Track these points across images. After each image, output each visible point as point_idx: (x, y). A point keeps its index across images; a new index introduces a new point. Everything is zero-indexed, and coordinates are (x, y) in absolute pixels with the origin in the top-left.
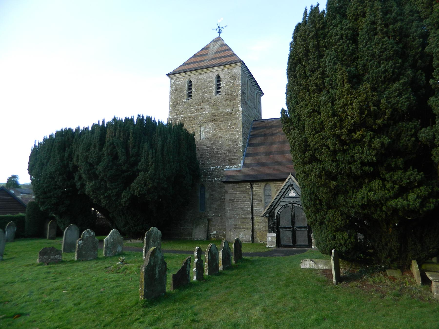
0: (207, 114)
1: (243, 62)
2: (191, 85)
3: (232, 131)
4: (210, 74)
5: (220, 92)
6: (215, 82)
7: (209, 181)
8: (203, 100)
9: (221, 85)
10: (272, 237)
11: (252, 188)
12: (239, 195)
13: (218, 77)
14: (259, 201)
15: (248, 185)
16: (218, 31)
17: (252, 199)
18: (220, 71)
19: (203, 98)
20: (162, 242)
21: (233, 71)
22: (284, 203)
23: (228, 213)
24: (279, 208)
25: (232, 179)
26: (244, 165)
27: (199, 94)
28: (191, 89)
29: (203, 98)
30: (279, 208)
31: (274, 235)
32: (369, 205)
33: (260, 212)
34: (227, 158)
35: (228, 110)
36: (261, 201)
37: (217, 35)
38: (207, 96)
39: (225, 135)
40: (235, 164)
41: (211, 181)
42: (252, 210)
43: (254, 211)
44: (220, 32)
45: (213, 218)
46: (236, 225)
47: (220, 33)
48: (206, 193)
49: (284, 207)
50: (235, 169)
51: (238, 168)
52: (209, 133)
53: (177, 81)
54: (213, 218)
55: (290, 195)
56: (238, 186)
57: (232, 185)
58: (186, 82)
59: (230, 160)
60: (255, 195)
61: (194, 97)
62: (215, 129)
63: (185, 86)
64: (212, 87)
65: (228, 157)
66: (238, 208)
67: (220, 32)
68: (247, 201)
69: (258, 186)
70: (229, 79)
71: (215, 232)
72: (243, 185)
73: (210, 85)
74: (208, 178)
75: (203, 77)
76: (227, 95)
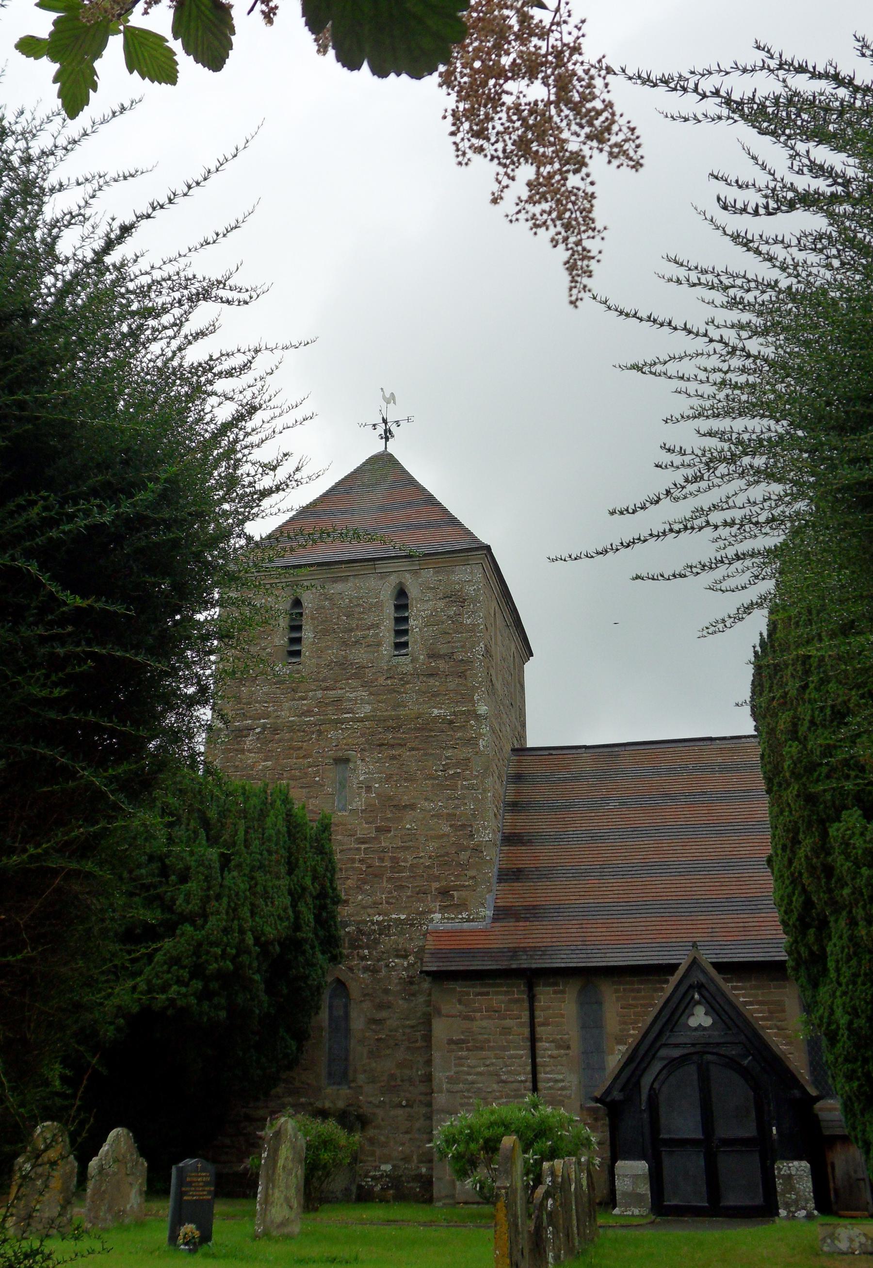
0: (361, 720)
1: (488, 548)
3: (454, 788)
4: (372, 582)
5: (405, 645)
6: (389, 611)
7: (366, 969)
8: (349, 672)
9: (411, 622)
10: (636, 1177)
11: (532, 999)
12: (484, 1023)
13: (401, 592)
14: (559, 1047)
15: (519, 992)
16: (381, 430)
17: (533, 1039)
18: (408, 575)
19: (343, 664)
21: (455, 578)
22: (676, 1053)
23: (440, 1091)
24: (657, 1066)
26: (502, 913)
27: (328, 647)
29: (343, 664)
30: (657, 1066)
31: (641, 1167)
33: (563, 1089)
34: (435, 885)
35: (436, 712)
36: (568, 1048)
37: (378, 447)
38: (359, 655)
39: (426, 799)
40: (462, 906)
41: (374, 971)
44: (387, 435)
45: (380, 1112)
47: (387, 439)
48: (353, 1014)
49: (674, 1064)
50: (466, 925)
52: (369, 789)
54: (380, 1112)
55: (693, 1022)
56: (478, 990)
57: (458, 987)
58: (283, 604)
59: (444, 893)
60: (543, 1024)
62: (389, 777)
64: (377, 626)
65: (437, 878)
67: (387, 435)
68: (516, 1048)
69: (555, 992)
70: (441, 604)
71: (387, 1168)
72: (501, 985)
73: (371, 619)
74: (363, 958)
75: (345, 590)
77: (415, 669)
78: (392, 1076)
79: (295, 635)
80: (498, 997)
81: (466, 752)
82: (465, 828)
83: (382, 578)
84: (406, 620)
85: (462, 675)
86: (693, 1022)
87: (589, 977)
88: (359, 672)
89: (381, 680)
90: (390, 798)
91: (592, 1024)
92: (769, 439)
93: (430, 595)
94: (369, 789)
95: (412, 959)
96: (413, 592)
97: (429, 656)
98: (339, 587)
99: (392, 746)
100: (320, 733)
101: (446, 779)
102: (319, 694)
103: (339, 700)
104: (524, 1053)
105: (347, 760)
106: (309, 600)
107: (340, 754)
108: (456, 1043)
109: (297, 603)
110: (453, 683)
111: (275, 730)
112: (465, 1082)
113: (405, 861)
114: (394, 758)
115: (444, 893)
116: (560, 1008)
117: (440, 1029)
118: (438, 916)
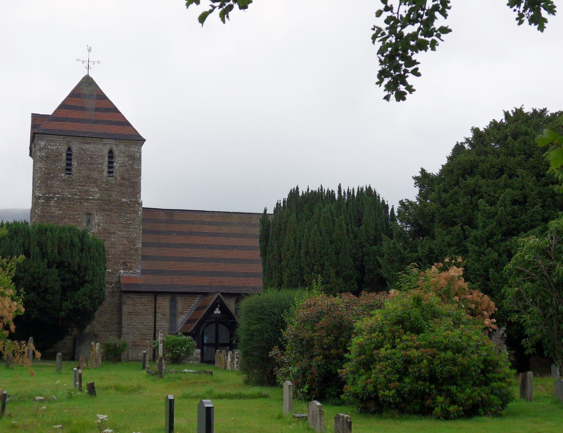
0: (96, 200)
2: (71, 155)
3: (129, 228)
4: (100, 146)
11: (155, 300)
12: (140, 307)
13: (111, 152)
15: (151, 298)
17: (155, 313)
18: (114, 146)
20: (63, 362)
21: (132, 149)
23: (125, 328)
25: (133, 289)
26: (143, 272)
28: (70, 160)
32: (502, 386)
34: (122, 261)
38: (95, 175)
40: (131, 269)
42: (155, 325)
43: (157, 326)
46: (135, 342)
51: (134, 274)
52: (99, 225)
53: (49, 145)
55: (215, 312)
57: (132, 296)
58: (64, 149)
60: (159, 308)
61: (76, 173)
62: (106, 222)
63: (61, 155)
64: (102, 164)
65: (122, 259)
66: (138, 323)
70: (126, 159)
73: (100, 161)
75: (90, 147)
76: (123, 178)
77: (116, 183)
78: (105, 323)
79: (69, 162)
80: (145, 299)
81: (134, 216)
82: (132, 242)
83: (104, 145)
84: (112, 162)
85: (133, 187)
86: (215, 312)
87: (173, 295)
88: (95, 181)
89: (103, 185)
90: (106, 229)
91: (173, 307)
92: (315, 204)
93: (122, 155)
94: (99, 225)
95: (113, 285)
96: (116, 152)
97: (121, 179)
98: (88, 146)
99: (108, 211)
100: (81, 203)
101: (127, 224)
102: (80, 187)
103: (87, 191)
104: (152, 317)
105: (91, 214)
106: (75, 149)
107: (88, 212)
108: (131, 313)
109: (69, 149)
110: (130, 190)
111: (63, 199)
112: (133, 325)
113: (111, 252)
114: (108, 215)
115: (125, 264)
116: (164, 303)
117: (125, 309)
118: (122, 271)
